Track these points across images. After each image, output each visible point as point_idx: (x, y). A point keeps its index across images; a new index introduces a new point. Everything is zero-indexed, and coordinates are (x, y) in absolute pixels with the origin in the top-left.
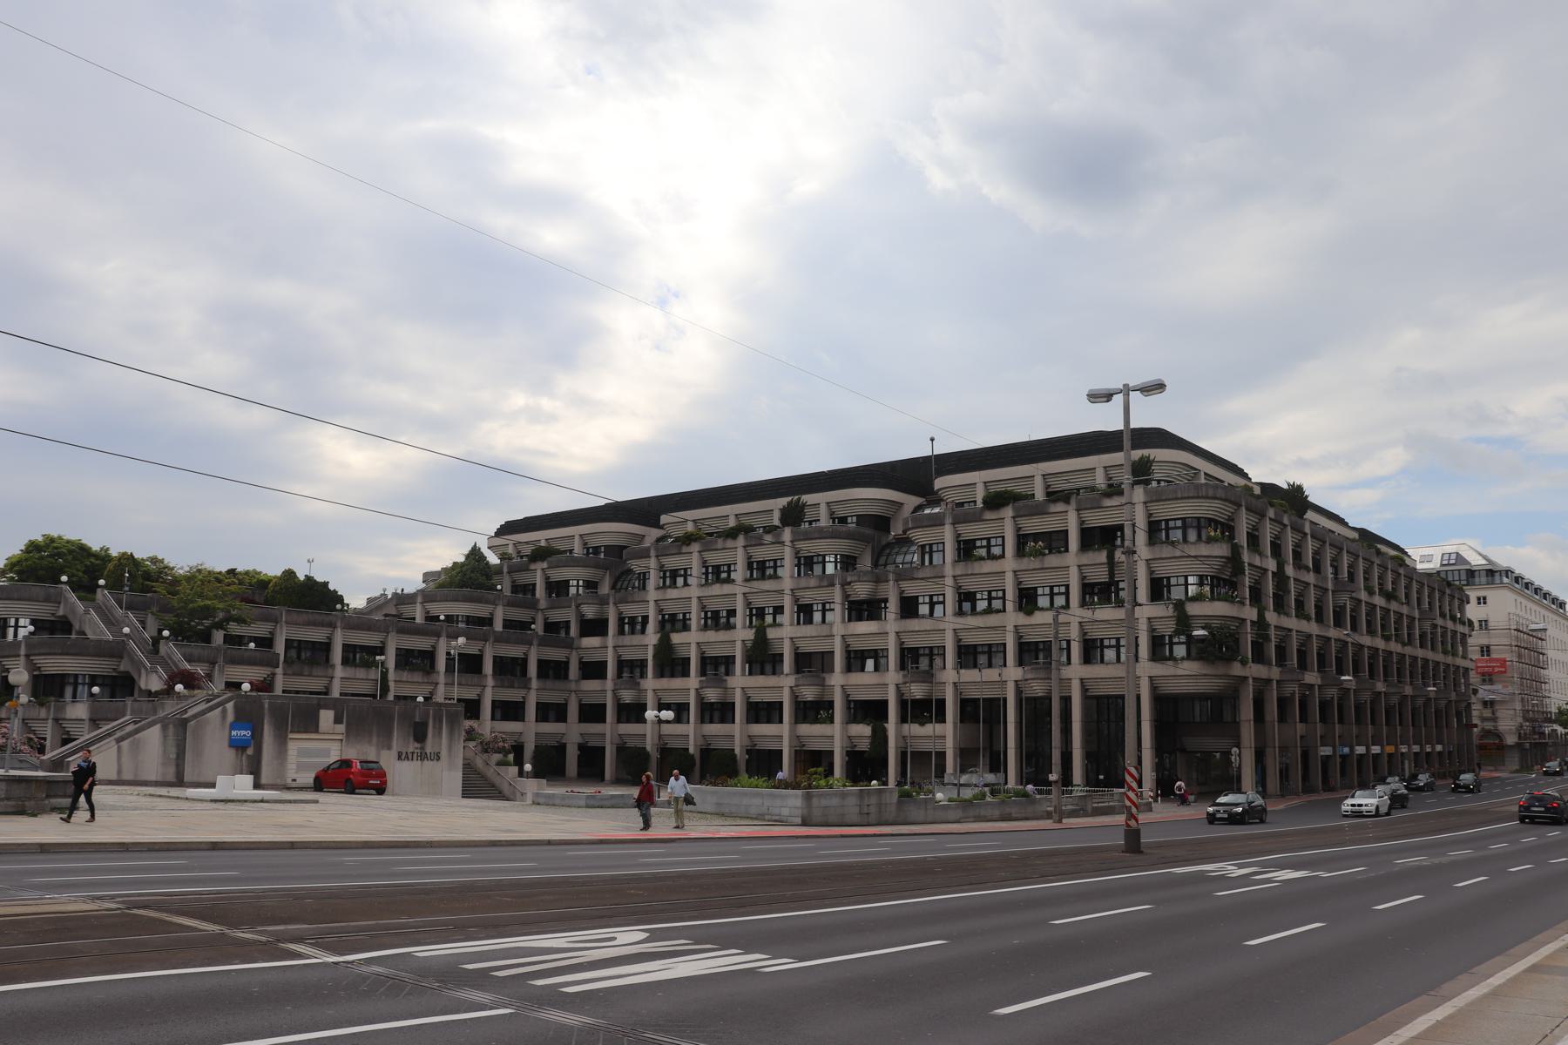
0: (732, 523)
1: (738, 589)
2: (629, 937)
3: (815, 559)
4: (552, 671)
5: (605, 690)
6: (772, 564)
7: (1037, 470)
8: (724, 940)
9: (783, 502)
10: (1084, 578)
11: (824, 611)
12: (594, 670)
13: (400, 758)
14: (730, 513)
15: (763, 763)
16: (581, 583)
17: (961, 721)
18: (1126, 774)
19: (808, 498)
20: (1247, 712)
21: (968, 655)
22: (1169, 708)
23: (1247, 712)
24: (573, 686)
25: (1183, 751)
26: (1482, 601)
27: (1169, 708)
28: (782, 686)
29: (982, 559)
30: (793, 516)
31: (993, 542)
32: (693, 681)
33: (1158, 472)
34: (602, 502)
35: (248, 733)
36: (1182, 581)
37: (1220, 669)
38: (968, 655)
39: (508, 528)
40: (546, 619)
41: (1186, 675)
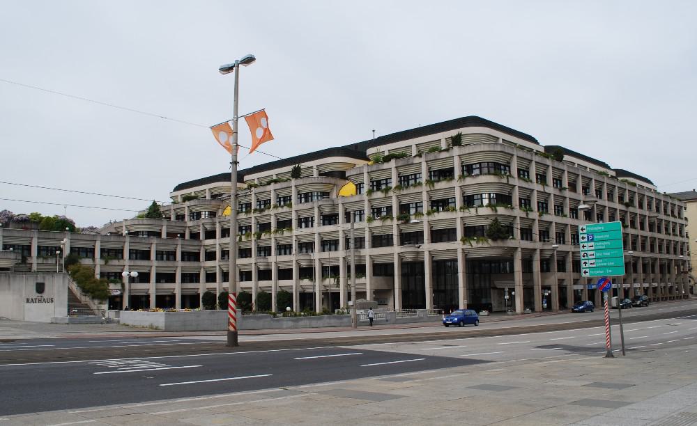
0: (386, 154)
1: (456, 183)
2: (137, 360)
3: (410, 177)
4: (191, 256)
5: (216, 265)
6: (413, 177)
7: (413, 142)
8: (157, 361)
9: (290, 168)
10: (431, 198)
11: (416, 207)
12: (211, 256)
13: (28, 301)
14: (273, 173)
15: (210, 300)
16: (207, 213)
17: (374, 276)
18: (235, 300)
19: (303, 165)
20: (518, 266)
21: (437, 236)
22: (474, 265)
23: (518, 266)
24: (202, 265)
25: (495, 288)
26: (165, 256)
27: (474, 265)
28: (251, 263)
29: (477, 175)
30: (296, 174)
31: (482, 165)
32: (341, 253)
33: (464, 141)
34: (277, 159)
35: (508, 263)
36: (479, 196)
37: (500, 243)
38: (437, 236)
39: (180, 187)
40: (191, 232)
41: (483, 248)
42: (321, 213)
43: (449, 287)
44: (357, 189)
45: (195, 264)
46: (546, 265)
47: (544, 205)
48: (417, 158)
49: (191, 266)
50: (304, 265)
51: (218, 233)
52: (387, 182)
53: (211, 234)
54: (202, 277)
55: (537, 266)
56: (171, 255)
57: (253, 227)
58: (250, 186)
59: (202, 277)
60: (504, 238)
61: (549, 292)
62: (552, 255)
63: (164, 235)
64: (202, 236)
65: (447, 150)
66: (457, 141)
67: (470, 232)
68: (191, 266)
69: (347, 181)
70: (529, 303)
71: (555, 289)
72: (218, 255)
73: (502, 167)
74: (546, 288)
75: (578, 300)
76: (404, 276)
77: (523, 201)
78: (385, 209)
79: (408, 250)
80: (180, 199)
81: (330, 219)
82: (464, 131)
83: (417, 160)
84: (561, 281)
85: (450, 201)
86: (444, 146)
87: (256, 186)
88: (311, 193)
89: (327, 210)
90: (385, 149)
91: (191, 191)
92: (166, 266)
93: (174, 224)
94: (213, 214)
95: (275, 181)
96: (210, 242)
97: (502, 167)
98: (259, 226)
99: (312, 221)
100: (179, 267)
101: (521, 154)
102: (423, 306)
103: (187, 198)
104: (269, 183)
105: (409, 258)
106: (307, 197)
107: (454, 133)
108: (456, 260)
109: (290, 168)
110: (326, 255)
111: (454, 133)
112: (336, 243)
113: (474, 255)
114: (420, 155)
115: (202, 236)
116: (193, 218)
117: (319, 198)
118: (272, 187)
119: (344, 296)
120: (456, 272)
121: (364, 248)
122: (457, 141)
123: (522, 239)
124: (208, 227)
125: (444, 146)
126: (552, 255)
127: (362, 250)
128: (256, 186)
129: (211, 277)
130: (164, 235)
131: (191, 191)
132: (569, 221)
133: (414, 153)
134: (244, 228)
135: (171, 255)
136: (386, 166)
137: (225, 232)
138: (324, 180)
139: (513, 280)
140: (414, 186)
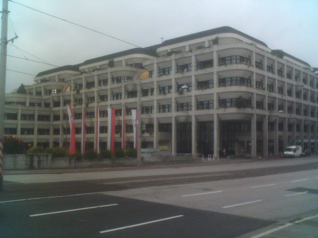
0: (169, 51)
9: (107, 62)
14: (97, 64)
16: (55, 90)
19: (116, 60)
20: (254, 126)
21: (201, 105)
23: (254, 126)
30: (111, 64)
33: (220, 41)
37: (242, 111)
38: (201, 105)
42: (126, 90)
43: (207, 141)
44: (150, 74)
45: (47, 123)
46: (271, 125)
47: (271, 87)
48: (190, 53)
49: (44, 124)
50: (88, 125)
51: (62, 104)
52: (169, 69)
53: (57, 104)
54: (51, 131)
55: (266, 127)
56: (31, 117)
57: (83, 100)
58: (82, 73)
59: (51, 131)
60: (245, 107)
61: (273, 144)
62: (276, 120)
63: (28, 104)
64: (51, 105)
65: (209, 47)
66: (216, 42)
67: (223, 103)
68: (44, 124)
69: (144, 70)
70: (260, 151)
71: (277, 142)
72: (61, 117)
73: (245, 60)
74: (270, 141)
75: (271, 149)
76: (178, 131)
77: (258, 83)
78: (167, 88)
79: (182, 114)
80: (39, 82)
81: (132, 94)
82: (221, 35)
83: (189, 54)
84: (280, 137)
85: (210, 82)
86: (207, 45)
87: (86, 72)
88: (121, 77)
89: (130, 88)
90: (168, 48)
91: (47, 76)
92: (27, 123)
93: (34, 97)
94: (59, 91)
95: (98, 70)
96: (57, 109)
97: (245, 60)
98: (99, 97)
99: (121, 95)
100: (36, 124)
101: (258, 51)
102: (190, 151)
103: (44, 81)
104: (94, 71)
105: (182, 120)
106: (118, 80)
107: (213, 37)
108: (212, 122)
109: (107, 62)
110: (162, 115)
111: (213, 37)
112: (169, 107)
113: (224, 118)
114: (191, 51)
115: (51, 105)
116: (47, 93)
117: (126, 80)
118: (96, 73)
119: (84, 148)
120: (212, 130)
121: (171, 112)
122: (216, 42)
123: (257, 108)
124: (56, 99)
125: (207, 45)
126: (276, 120)
127: (93, 119)
128: (86, 72)
129: (56, 132)
130: (28, 104)
131: (47, 76)
132: (287, 98)
133: (187, 49)
134: (78, 100)
135: (31, 117)
136: (168, 59)
137: (67, 102)
138: (129, 68)
139: (250, 135)
140: (38, 80)
